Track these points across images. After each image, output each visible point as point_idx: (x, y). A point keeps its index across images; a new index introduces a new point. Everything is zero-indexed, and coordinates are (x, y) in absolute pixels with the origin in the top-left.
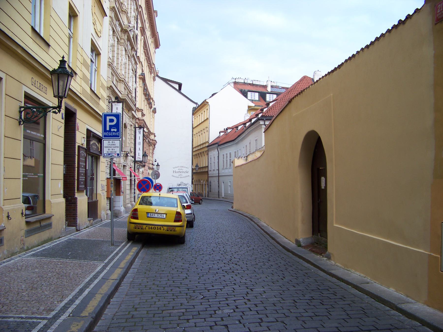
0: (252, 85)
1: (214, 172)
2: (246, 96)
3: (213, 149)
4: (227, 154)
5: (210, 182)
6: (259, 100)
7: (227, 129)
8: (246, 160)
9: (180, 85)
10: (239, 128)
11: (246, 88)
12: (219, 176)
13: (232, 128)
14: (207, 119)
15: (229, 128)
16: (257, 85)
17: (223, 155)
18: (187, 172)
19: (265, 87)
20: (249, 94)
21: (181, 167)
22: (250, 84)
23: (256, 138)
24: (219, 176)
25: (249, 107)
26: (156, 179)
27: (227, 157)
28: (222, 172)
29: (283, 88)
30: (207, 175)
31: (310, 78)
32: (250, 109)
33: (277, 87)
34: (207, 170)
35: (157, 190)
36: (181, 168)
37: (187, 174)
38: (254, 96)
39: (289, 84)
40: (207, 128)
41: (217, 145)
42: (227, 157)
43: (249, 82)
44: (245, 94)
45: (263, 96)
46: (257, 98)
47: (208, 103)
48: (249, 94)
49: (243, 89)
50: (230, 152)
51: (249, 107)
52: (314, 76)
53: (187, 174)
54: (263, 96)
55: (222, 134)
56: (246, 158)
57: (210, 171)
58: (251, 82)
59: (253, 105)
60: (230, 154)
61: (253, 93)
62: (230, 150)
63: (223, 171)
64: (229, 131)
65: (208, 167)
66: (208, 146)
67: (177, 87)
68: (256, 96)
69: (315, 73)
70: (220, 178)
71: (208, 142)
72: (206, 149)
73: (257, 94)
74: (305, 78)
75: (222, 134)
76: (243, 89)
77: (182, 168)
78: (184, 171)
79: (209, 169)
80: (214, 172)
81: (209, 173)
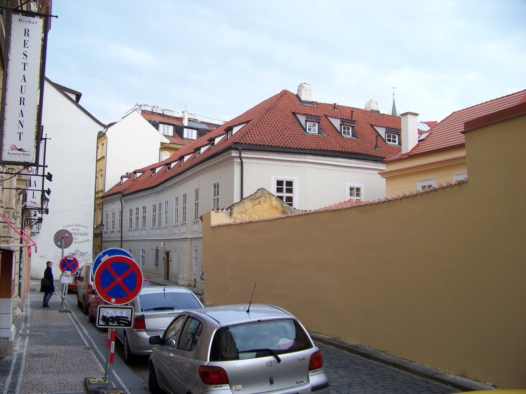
0: (163, 115)
1: (113, 235)
2: (157, 128)
3: (113, 201)
4: (137, 209)
6: (173, 137)
7: (135, 173)
8: (231, 214)
9: (79, 96)
10: (157, 170)
11: (158, 119)
12: (121, 241)
13: (143, 171)
14: (103, 158)
15: (139, 171)
16: (169, 117)
17: (131, 211)
18: (86, 234)
19: (181, 119)
20: (161, 126)
21: (76, 225)
22: (160, 114)
23: (216, 181)
24: (121, 241)
25: (162, 144)
26: (66, 247)
27: (137, 213)
28: (128, 235)
29: (203, 123)
30: (100, 239)
31: (292, 93)
32: (164, 147)
33: (195, 121)
35: (68, 270)
36: (76, 228)
37: (86, 238)
38: (168, 130)
39: (221, 117)
40: (102, 170)
41: (120, 195)
42: (137, 213)
43: (158, 112)
44: (156, 125)
45: (179, 131)
46: (171, 133)
48: (161, 126)
49: (156, 119)
50: (144, 205)
51: (162, 144)
52: (298, 91)
53: (86, 238)
54: (179, 131)
55: (125, 180)
56: (229, 210)
57: (106, 232)
58: (161, 112)
59: (168, 141)
60: (145, 208)
61: (166, 126)
62: (147, 202)
63: (130, 234)
64: (138, 175)
66: (103, 197)
67: (74, 97)
68: (170, 130)
69: (301, 86)
71: (102, 191)
73: (171, 128)
74: (285, 93)
75: (125, 180)
76: (156, 119)
77: (78, 228)
78: (81, 232)
79: (105, 230)
80: (113, 235)
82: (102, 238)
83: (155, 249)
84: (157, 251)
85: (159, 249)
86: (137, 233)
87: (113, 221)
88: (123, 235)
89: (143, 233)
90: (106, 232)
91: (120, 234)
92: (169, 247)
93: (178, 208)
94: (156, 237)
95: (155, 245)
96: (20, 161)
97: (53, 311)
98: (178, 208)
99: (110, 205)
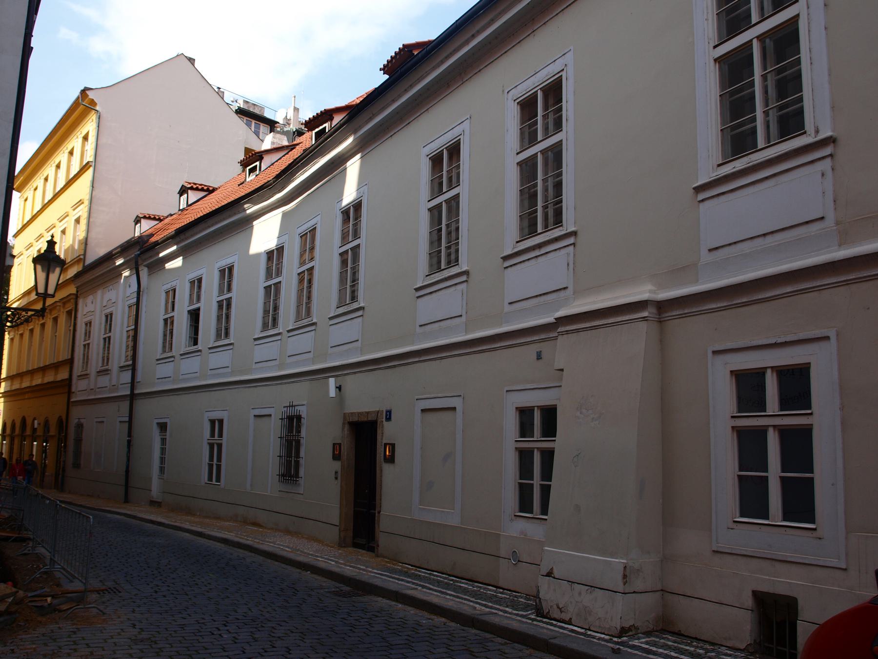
5: (80, 426)
24: (133, 397)
28: (157, 374)
34: (63, 375)
47: (93, 103)
63: (165, 370)
65: (70, 362)
70: (143, 408)
72: (72, 289)
81: (79, 386)
82: (70, 393)
83: (277, 413)
84: (293, 422)
85: (303, 411)
86: (191, 365)
87: (107, 340)
88: (139, 378)
89: (222, 359)
90: (84, 376)
91: (127, 376)
92: (364, 396)
93: (201, 305)
94: (281, 366)
95: (275, 401)
96: (377, 86)
97: (269, 561)
98: (175, 314)
99: (99, 292)
